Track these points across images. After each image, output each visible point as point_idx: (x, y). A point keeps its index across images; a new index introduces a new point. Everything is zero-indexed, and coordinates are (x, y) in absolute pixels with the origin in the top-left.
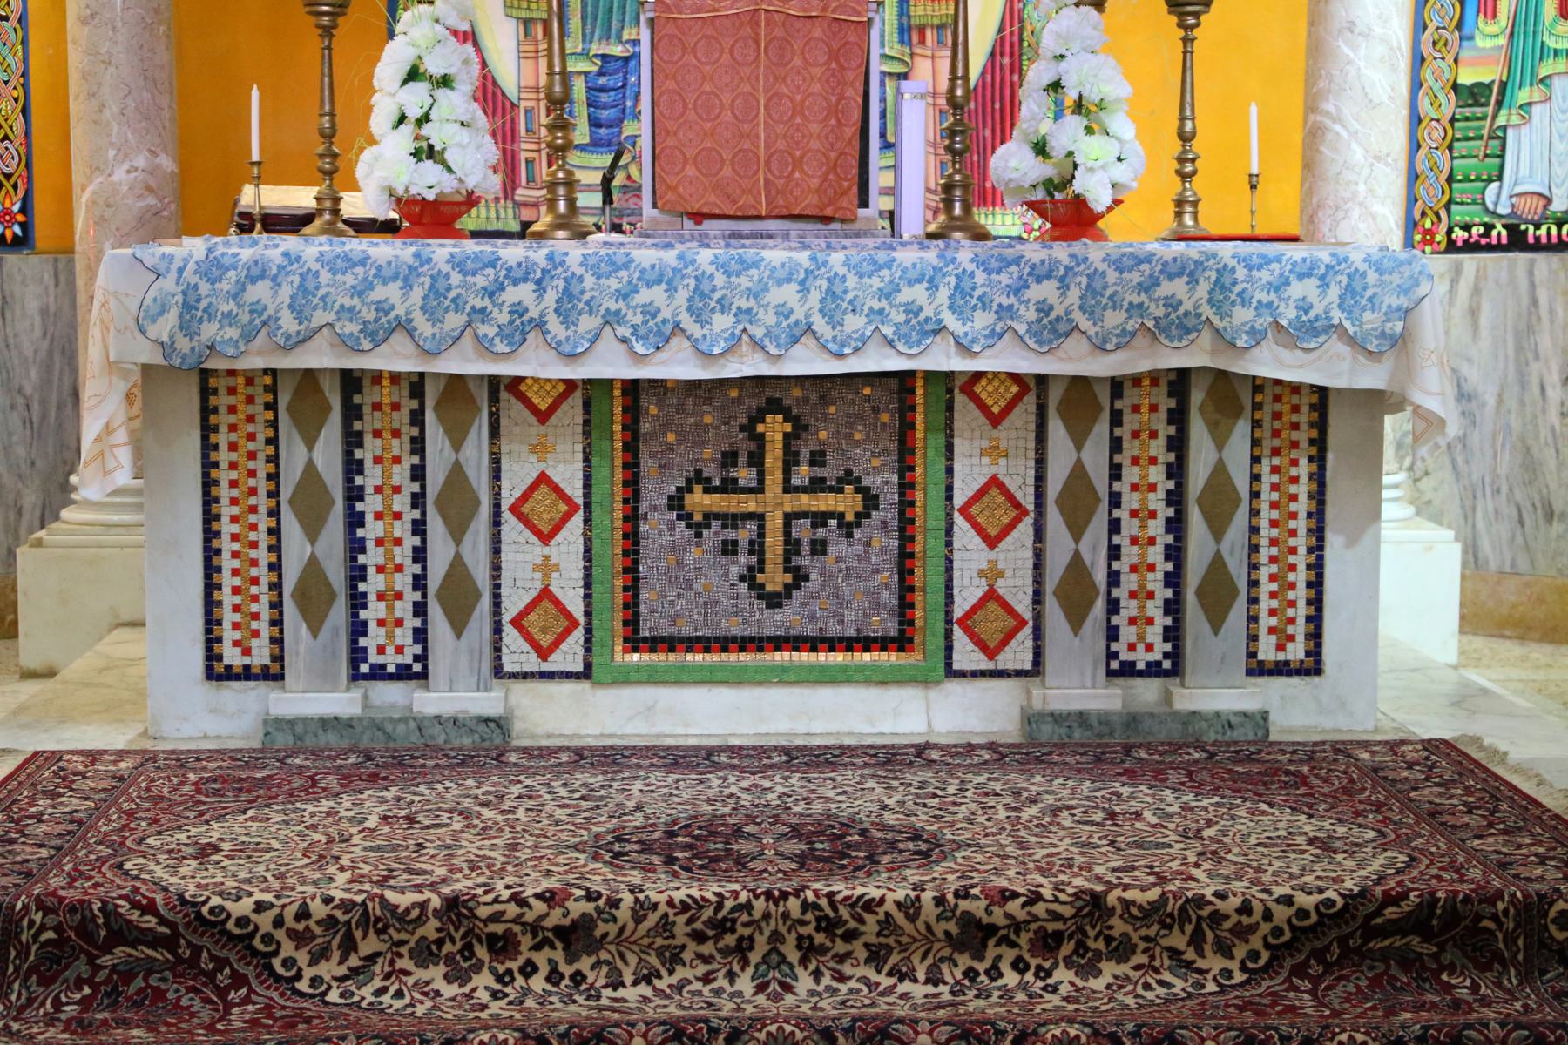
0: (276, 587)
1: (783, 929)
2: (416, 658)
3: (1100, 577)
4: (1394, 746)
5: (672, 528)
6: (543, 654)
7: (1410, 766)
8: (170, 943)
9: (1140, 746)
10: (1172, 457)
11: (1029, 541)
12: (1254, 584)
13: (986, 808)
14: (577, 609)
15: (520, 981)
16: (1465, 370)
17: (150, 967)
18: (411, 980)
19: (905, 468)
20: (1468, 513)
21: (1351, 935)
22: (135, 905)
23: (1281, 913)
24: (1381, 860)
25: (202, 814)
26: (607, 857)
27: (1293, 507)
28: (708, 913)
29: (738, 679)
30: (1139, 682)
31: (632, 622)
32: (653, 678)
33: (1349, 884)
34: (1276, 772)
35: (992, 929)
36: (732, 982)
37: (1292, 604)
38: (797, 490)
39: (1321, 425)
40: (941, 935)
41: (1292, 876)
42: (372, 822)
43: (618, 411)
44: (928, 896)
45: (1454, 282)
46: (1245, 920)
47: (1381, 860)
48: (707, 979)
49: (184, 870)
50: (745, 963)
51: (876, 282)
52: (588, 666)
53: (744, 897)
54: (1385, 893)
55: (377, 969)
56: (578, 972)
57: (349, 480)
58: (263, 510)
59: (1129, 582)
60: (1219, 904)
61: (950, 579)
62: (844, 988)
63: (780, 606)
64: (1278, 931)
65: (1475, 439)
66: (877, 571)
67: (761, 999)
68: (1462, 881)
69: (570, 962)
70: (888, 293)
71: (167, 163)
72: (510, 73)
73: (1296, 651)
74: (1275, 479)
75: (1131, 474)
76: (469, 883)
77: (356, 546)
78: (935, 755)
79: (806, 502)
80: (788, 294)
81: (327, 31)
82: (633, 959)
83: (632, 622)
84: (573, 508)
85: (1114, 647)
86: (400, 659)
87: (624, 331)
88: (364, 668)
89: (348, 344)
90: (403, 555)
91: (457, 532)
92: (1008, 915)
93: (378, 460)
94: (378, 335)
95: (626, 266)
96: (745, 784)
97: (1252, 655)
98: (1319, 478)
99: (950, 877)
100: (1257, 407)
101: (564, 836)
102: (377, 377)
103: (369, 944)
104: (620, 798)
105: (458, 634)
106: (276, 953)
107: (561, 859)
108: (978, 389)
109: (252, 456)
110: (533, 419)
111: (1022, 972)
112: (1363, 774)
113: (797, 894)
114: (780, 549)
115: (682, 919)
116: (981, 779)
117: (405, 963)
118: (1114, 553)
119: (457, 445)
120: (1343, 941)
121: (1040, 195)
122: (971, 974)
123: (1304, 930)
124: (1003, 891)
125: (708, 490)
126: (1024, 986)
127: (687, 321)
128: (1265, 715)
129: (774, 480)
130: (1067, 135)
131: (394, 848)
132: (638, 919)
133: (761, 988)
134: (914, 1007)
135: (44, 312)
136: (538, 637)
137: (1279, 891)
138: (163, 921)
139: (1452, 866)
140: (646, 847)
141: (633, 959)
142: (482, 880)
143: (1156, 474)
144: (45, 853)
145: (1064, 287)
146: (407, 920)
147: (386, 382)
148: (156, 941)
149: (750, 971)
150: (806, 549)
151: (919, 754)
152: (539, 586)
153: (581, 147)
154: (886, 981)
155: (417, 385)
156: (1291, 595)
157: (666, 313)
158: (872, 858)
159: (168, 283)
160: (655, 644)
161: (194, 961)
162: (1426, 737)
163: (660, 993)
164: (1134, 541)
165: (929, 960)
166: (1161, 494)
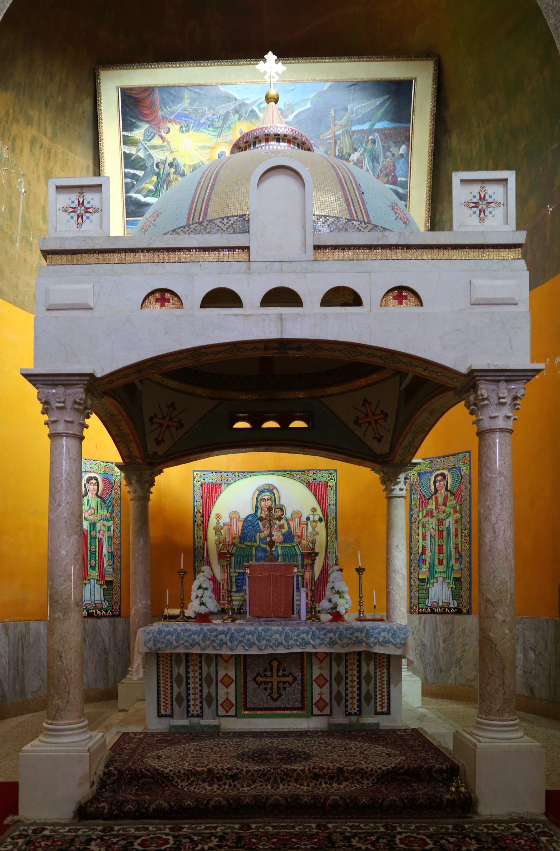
0: (172, 698)
3: (344, 695)
4: (405, 730)
5: (254, 685)
6: (227, 712)
7: (408, 735)
8: (152, 778)
11: (329, 687)
12: (376, 695)
13: (320, 747)
14: (234, 702)
15: (223, 786)
16: (423, 639)
19: (302, 672)
20: (425, 671)
22: (146, 770)
23: (379, 771)
26: (241, 759)
28: (261, 772)
31: (245, 705)
33: (393, 765)
35: (320, 775)
37: (384, 699)
39: (389, 662)
41: (382, 763)
42: (192, 750)
43: (242, 661)
44: (307, 768)
45: (420, 621)
48: (261, 786)
49: (155, 762)
51: (295, 633)
52: (236, 714)
53: (269, 769)
54: (400, 767)
57: (186, 675)
58: (169, 681)
59: (350, 695)
60: (367, 770)
62: (289, 788)
64: (378, 775)
66: (297, 693)
68: (416, 763)
70: (298, 636)
71: (149, 602)
72: (218, 576)
73: (385, 709)
75: (350, 673)
77: (188, 689)
78: (309, 734)
80: (277, 636)
81: (182, 578)
82: (246, 782)
83: (245, 705)
84: (233, 681)
86: (197, 713)
87: (243, 644)
88: (190, 715)
89: (186, 648)
91: (209, 687)
94: (193, 645)
95: (244, 631)
97: (376, 710)
98: (389, 673)
100: (375, 658)
102: (192, 654)
103: (192, 779)
104: (243, 745)
107: (231, 760)
109: (167, 670)
110: (224, 662)
113: (280, 768)
114: (276, 689)
115: (256, 774)
116: (319, 740)
117: (200, 782)
118: (347, 689)
119: (209, 668)
121: (330, 611)
122: (316, 785)
124: (322, 767)
125: (261, 677)
126: (327, 787)
127: (256, 642)
128: (378, 724)
129: (275, 674)
130: (336, 598)
131: (197, 757)
132: (247, 774)
133: (272, 788)
134: (304, 792)
135: (123, 630)
137: (379, 766)
139: (415, 761)
140: (249, 757)
141: (246, 782)
143: (355, 672)
144: (127, 757)
145: (335, 634)
146: (200, 773)
150: (282, 689)
152: (226, 697)
153: (234, 592)
154: (298, 786)
155: (201, 655)
157: (252, 640)
158: (295, 759)
159: (151, 635)
162: (412, 728)
163: (252, 789)
164: (351, 687)
166: (356, 676)
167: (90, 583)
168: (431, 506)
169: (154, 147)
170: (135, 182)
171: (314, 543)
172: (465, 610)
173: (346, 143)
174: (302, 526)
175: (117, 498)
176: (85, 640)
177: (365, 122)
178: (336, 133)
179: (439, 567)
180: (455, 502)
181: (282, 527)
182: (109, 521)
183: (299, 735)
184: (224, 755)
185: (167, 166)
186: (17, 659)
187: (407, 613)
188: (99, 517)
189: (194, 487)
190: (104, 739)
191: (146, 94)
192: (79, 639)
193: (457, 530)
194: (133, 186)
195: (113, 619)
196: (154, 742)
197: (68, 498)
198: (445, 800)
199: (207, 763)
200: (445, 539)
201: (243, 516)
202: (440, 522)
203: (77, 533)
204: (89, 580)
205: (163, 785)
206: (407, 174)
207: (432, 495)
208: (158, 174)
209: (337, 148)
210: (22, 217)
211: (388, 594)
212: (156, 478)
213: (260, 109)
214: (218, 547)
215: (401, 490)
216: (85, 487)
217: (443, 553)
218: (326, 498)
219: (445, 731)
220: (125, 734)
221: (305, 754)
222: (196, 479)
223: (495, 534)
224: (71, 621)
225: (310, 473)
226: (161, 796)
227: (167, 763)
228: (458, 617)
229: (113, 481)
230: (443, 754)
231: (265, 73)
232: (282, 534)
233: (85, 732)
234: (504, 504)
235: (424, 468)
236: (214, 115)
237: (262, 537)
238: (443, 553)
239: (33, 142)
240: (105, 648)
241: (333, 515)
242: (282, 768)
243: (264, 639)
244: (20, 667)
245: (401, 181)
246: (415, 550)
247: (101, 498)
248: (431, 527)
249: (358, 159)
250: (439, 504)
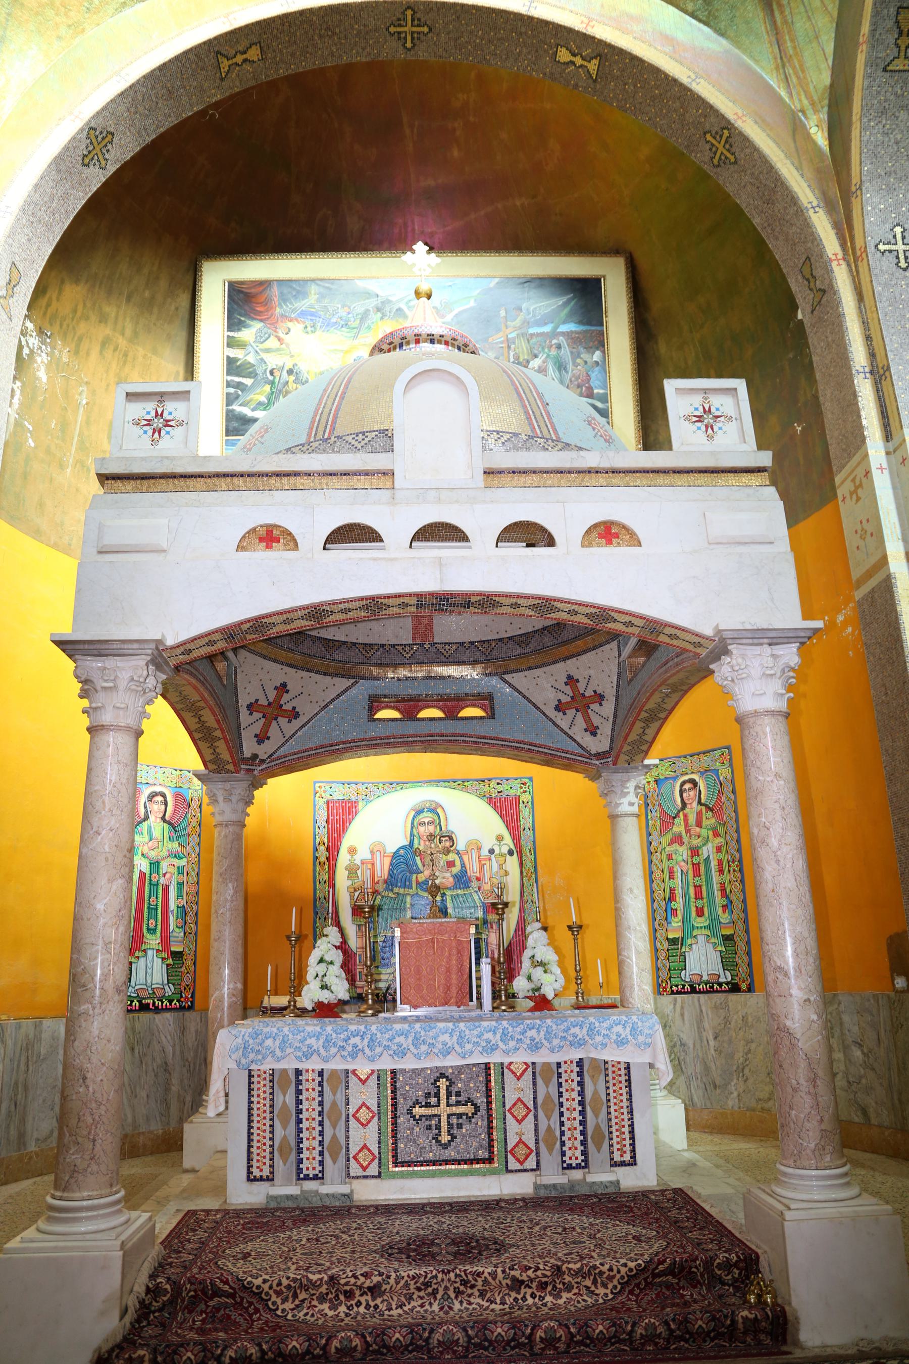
0: (272, 1146)
1: (448, 1285)
2: (320, 1172)
5: (408, 1121)
6: (364, 1169)
7: (668, 1200)
8: (232, 1296)
9: (576, 1196)
10: (579, 1088)
15: (355, 1309)
16: (682, 1035)
17: (226, 1306)
18: (317, 1309)
20: (688, 1087)
21: (648, 1277)
22: (222, 1281)
23: (623, 1270)
24: (657, 1245)
25: (245, 1238)
27: (622, 1104)
28: (422, 1279)
29: (433, 1175)
30: (573, 1171)
32: (402, 1175)
34: (622, 1206)
35: (522, 1282)
36: (431, 1307)
38: (452, 1105)
40: (504, 1285)
41: (627, 1254)
45: (675, 1005)
46: (611, 1274)
47: (657, 1245)
48: (422, 1306)
50: (435, 1298)
52: (380, 1173)
53: (434, 1272)
55: (305, 1305)
56: (376, 1305)
59: (568, 1134)
61: (506, 1136)
62: (471, 1307)
63: (447, 1148)
64: (623, 1277)
65: (688, 1059)
67: (441, 1313)
68: (684, 1253)
69: (373, 1301)
72: (354, 943)
74: (615, 1094)
76: (337, 1269)
78: (503, 1204)
79: (455, 1110)
82: (395, 1299)
83: (395, 1156)
85: (564, 1158)
88: (302, 1176)
90: (315, 1133)
92: (528, 1276)
93: (307, 1099)
94: (307, 1056)
96: (435, 1220)
99: (508, 1261)
101: (371, 1246)
103: (302, 1295)
104: (391, 1228)
105: (334, 1163)
106: (269, 1300)
107: (370, 1258)
108: (512, 1067)
111: (534, 1298)
112: (652, 1206)
115: (412, 1282)
116: (519, 1215)
117: (315, 1303)
118: (562, 1124)
120: (645, 1279)
121: (530, 994)
122: (516, 1299)
123: (631, 1276)
124: (526, 1266)
128: (618, 1182)
129: (443, 1103)
131: (311, 1254)
132: (397, 1283)
133: (441, 1309)
135: (196, 1031)
136: (362, 1163)
138: (231, 1288)
140: (400, 1251)
141: (395, 1299)
142: (342, 1268)
144: (191, 1257)
146: (315, 1285)
147: (310, 1072)
148: (229, 1296)
149: (437, 1302)
150: (455, 1126)
151: (497, 1204)
154: (486, 1304)
156: (624, 1136)
158: (480, 1254)
160: (403, 1164)
161: (241, 1303)
165: (501, 1295)
167: (146, 955)
168: (679, 827)
169: (268, 351)
170: (240, 393)
171: (502, 887)
172: (744, 986)
173: (523, 349)
174: (483, 862)
175: (194, 823)
176: (133, 1049)
177: (546, 324)
178: (510, 336)
179: (699, 919)
180: (713, 820)
181: (451, 864)
182: (181, 858)
183: (487, 1208)
184: (358, 1249)
185: (285, 373)
186: (16, 1084)
187: (654, 994)
188: (165, 853)
189: (315, 806)
190: (152, 1223)
191: (261, 289)
192: (118, 1048)
193: (720, 862)
194: (237, 397)
195: (181, 1014)
196: (239, 1227)
197: (113, 822)
198: (740, 1320)
199: (328, 1264)
200: (703, 877)
201: (391, 849)
202: (695, 852)
203: (123, 876)
204: (145, 951)
205: (251, 1310)
206: (606, 384)
207: (679, 812)
208: (272, 383)
209: (512, 354)
210: (79, 435)
211: (621, 964)
212: (255, 793)
213: (409, 308)
214: (352, 897)
215: (631, 804)
216: (145, 807)
217: (702, 898)
218: (518, 820)
219: (730, 1191)
220: (191, 1214)
221: (496, 1243)
222: (318, 795)
223: (778, 865)
224: (106, 1018)
225: (493, 783)
226: (246, 1332)
227: (259, 1267)
228: (733, 997)
229: (189, 798)
230: (730, 1232)
231: (414, 265)
232: (452, 876)
233: (119, 1211)
234: (788, 821)
235: (664, 771)
236: (349, 313)
237: (420, 880)
238: (702, 898)
239: (104, 344)
240: (166, 1063)
241: (530, 845)
242: (458, 1271)
243: (424, 1042)
244: (19, 1096)
245: (598, 393)
246: (659, 894)
247: (169, 823)
248: (680, 858)
249: (540, 367)
250: (690, 824)
